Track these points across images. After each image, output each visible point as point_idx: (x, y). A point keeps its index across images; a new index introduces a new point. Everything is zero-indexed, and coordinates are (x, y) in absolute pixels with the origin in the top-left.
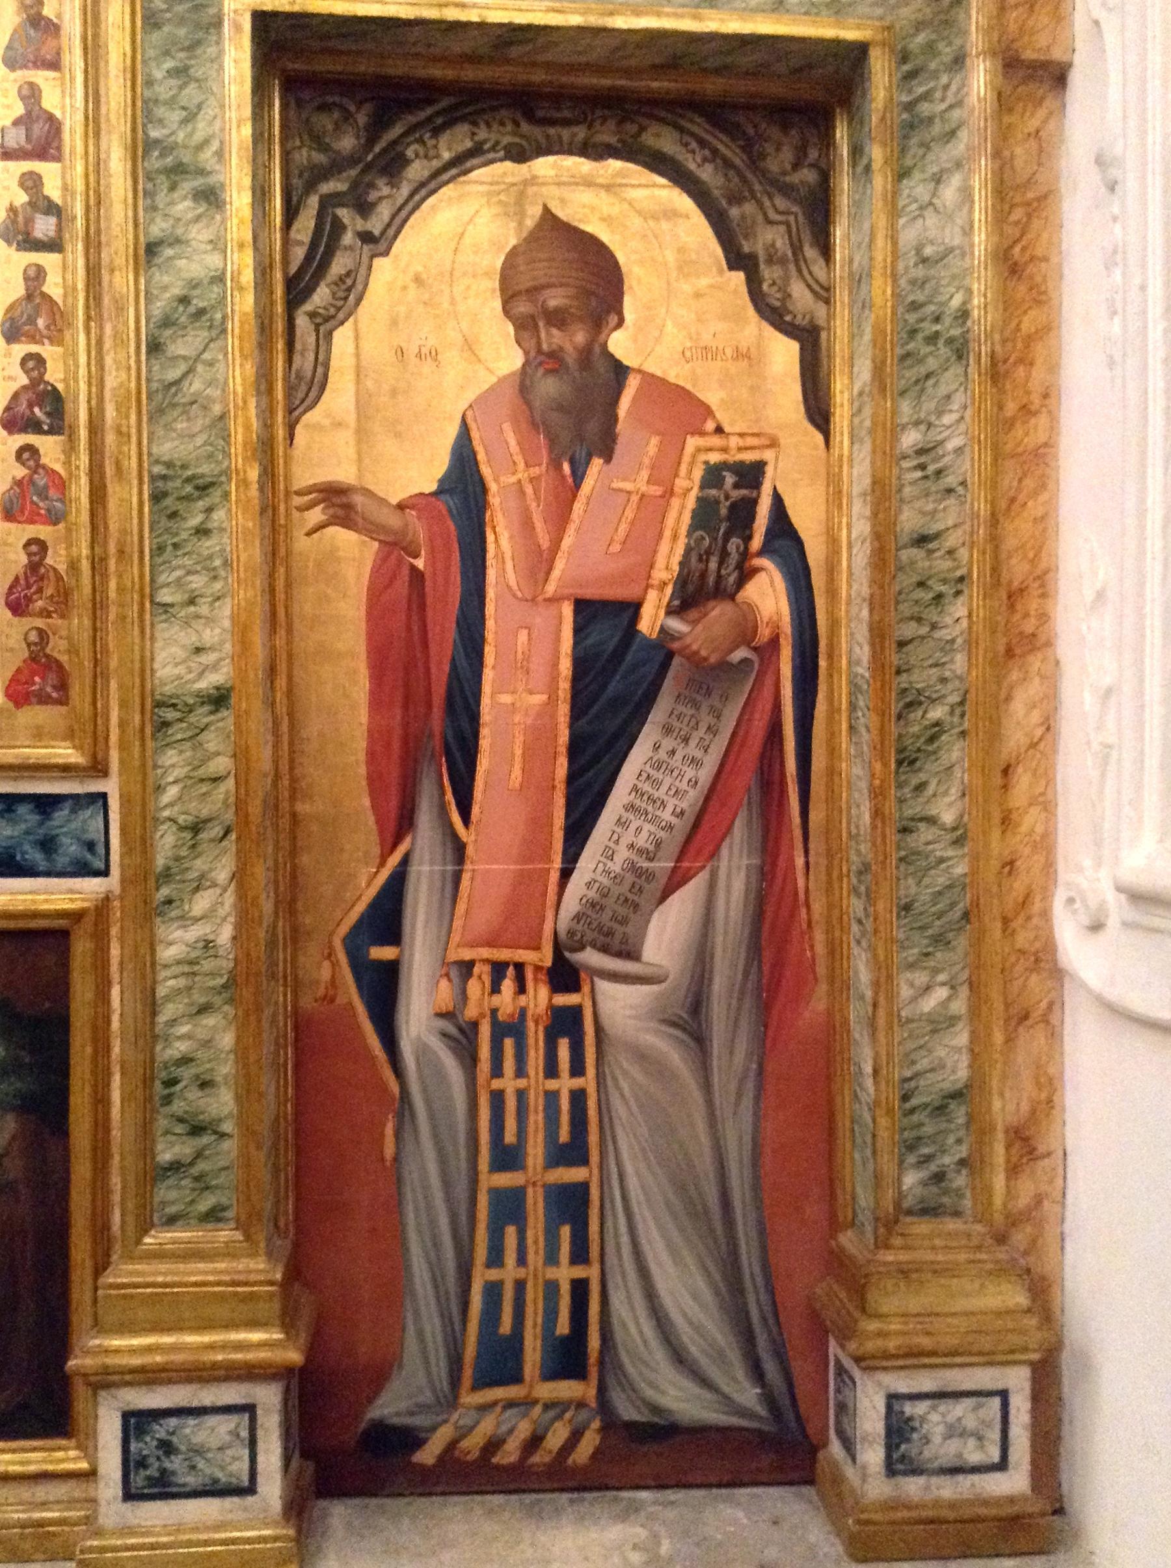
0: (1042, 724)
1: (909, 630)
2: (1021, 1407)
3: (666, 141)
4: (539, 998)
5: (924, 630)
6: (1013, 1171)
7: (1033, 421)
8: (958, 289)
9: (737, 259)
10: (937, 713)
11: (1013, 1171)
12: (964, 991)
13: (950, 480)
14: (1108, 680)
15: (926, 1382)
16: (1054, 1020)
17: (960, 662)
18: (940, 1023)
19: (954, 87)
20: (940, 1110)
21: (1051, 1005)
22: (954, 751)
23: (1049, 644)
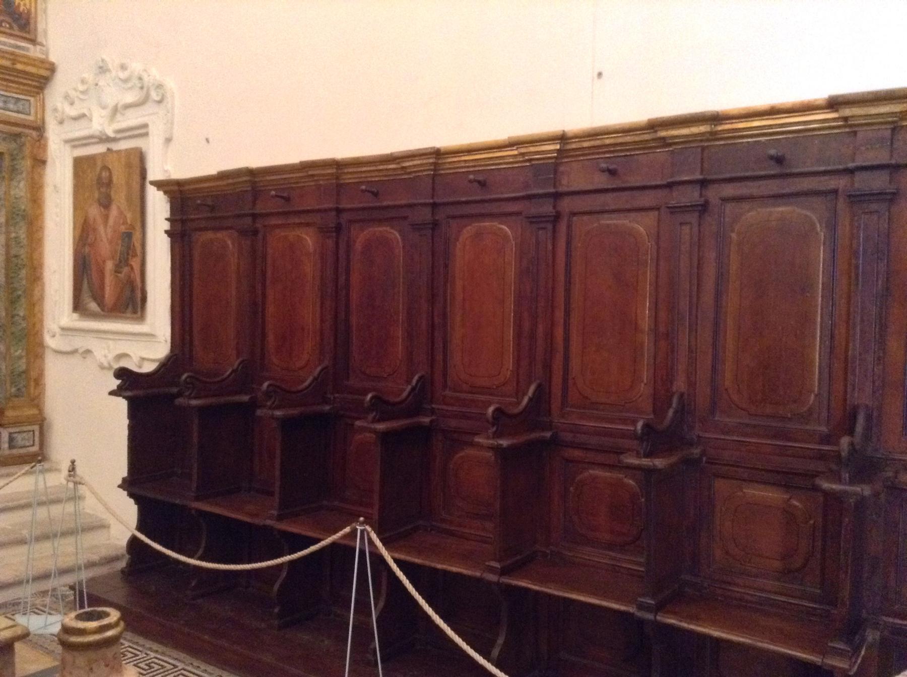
1: (13, 275)
2: (37, 433)
5: (16, 275)
6: (35, 388)
10: (20, 293)
11: (35, 388)
12: (25, 351)
13: (21, 244)
15: (17, 430)
17: (24, 282)
18: (20, 358)
20: (19, 375)
22: (23, 300)
23: (42, 279)
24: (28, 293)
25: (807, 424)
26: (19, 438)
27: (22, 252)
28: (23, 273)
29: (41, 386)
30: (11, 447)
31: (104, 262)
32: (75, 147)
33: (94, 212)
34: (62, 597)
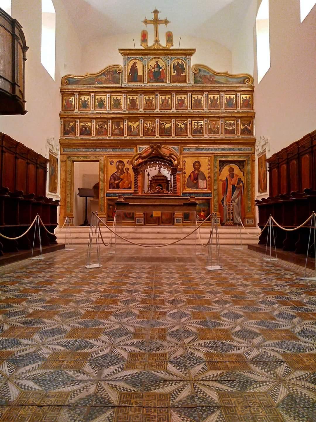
3: (236, 163)
4: (230, 203)
9: (240, 168)
18: (250, 203)
22: (250, 191)
24: (252, 190)
25: (12, 347)
26: (249, 221)
27: (250, 181)
28: (250, 185)
30: (247, 223)
33: (260, 169)
34: (208, 212)
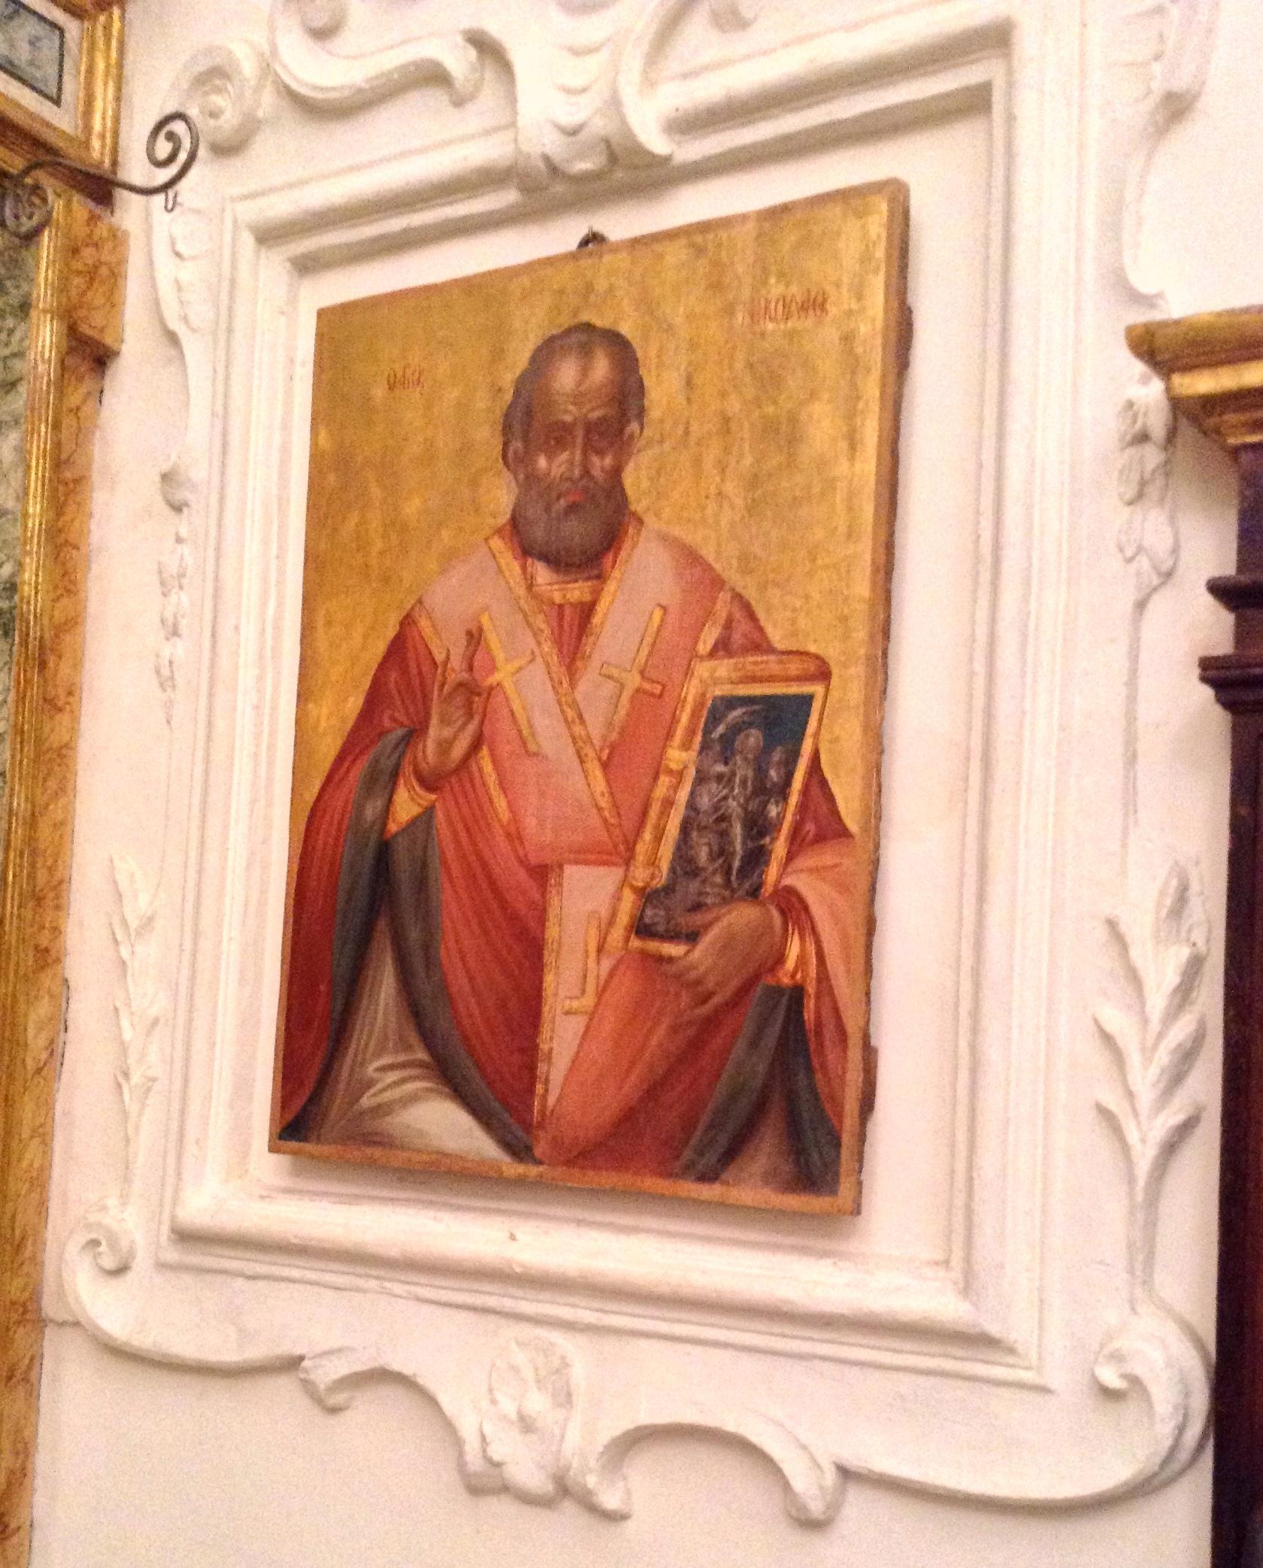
0: (47, 1048)
7: (58, 717)
8: (8, 558)
14: (154, 1011)
16: (33, 1376)
19: (18, 335)
21: (32, 1359)
23: (58, 960)
29: (15, 1540)
31: (543, 874)
32: (307, 266)
